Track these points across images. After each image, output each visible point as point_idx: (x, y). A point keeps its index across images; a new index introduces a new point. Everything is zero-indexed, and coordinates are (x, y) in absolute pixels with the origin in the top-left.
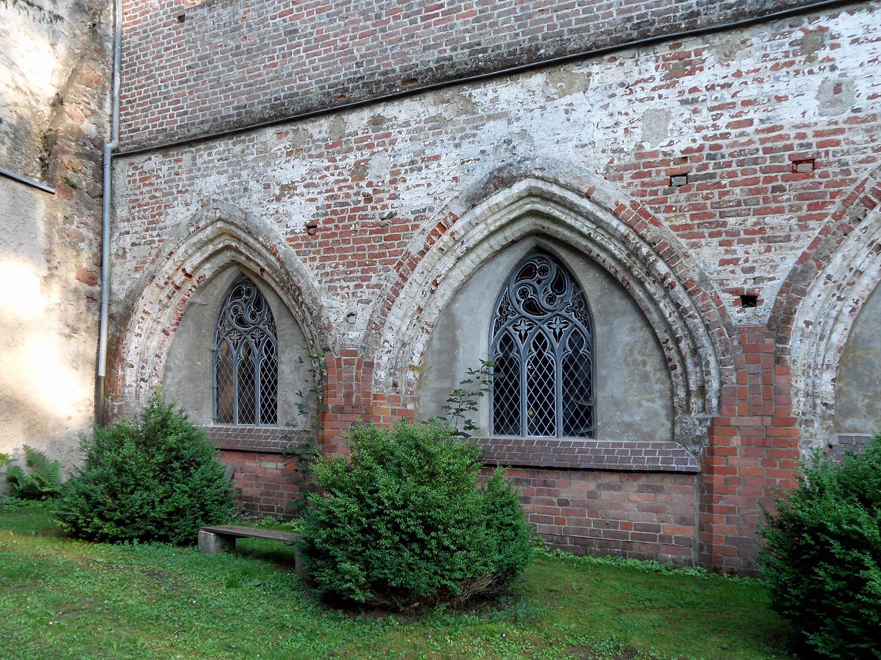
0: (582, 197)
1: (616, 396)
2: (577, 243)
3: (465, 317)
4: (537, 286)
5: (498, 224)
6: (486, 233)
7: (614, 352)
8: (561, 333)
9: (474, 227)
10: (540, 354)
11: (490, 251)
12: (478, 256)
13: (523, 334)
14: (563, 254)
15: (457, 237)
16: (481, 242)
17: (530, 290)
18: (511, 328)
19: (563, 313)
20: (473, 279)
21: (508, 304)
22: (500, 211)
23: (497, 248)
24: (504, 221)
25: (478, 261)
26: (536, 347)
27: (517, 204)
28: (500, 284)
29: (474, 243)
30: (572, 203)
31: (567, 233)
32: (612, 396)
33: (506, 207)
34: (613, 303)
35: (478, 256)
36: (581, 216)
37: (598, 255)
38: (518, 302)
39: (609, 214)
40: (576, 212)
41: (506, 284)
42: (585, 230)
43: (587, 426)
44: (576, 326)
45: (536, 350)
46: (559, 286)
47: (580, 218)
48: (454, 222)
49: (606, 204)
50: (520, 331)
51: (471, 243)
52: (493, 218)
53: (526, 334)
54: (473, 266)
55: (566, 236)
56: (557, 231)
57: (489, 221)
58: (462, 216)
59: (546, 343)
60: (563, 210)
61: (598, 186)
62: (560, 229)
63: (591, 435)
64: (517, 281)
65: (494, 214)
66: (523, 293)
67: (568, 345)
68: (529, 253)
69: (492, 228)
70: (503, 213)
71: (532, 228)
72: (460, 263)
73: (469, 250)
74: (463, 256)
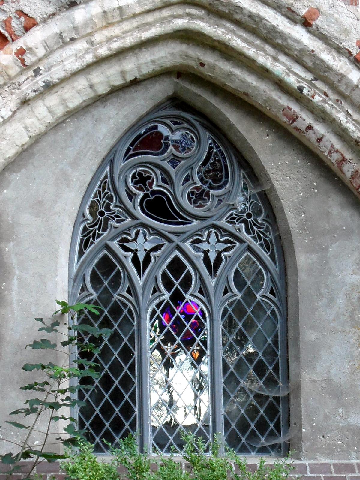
0: (294, 21)
1: (336, 380)
2: (269, 100)
3: (26, 218)
4: (172, 171)
5: (116, 45)
6: (89, 58)
7: (331, 300)
8: (219, 260)
9: (65, 44)
10: (177, 298)
11: (89, 94)
12: (64, 102)
13: (141, 257)
14: (233, 117)
15: (29, 59)
16: (75, 74)
17: (156, 176)
18: (115, 245)
19: (223, 223)
20: (44, 143)
21: (110, 199)
22: (122, 21)
23: (102, 90)
24: (129, 41)
25: (60, 111)
26: (169, 285)
27: (157, 15)
28: (98, 160)
29: (62, 74)
30: (273, 30)
31: (251, 80)
32: (329, 380)
33: (135, 16)
34: (328, 214)
35: (64, 102)
36: (286, 54)
37: (310, 127)
38: (131, 196)
39: (344, 60)
40: (275, 46)
41: (109, 160)
42: (292, 80)
43: (272, 435)
44: (250, 249)
45: (168, 289)
46: (215, 175)
47: (282, 58)
48: (27, 29)
49: (341, 41)
50: (135, 252)
51: (56, 74)
52: (108, 33)
53: (147, 259)
54: (49, 119)
55: (249, 86)
56: (230, 75)
57: (98, 37)
58: (44, 21)
59: (188, 278)
60: (251, 38)
61: (325, 8)
62: (237, 71)
63: (284, 450)
64: (127, 155)
65: (109, 25)
66: (142, 180)
67: (232, 284)
68: (158, 107)
69: (104, 51)
70: (127, 26)
71: (179, 61)
72: (25, 111)
73: (49, 87)
74: (35, 98)
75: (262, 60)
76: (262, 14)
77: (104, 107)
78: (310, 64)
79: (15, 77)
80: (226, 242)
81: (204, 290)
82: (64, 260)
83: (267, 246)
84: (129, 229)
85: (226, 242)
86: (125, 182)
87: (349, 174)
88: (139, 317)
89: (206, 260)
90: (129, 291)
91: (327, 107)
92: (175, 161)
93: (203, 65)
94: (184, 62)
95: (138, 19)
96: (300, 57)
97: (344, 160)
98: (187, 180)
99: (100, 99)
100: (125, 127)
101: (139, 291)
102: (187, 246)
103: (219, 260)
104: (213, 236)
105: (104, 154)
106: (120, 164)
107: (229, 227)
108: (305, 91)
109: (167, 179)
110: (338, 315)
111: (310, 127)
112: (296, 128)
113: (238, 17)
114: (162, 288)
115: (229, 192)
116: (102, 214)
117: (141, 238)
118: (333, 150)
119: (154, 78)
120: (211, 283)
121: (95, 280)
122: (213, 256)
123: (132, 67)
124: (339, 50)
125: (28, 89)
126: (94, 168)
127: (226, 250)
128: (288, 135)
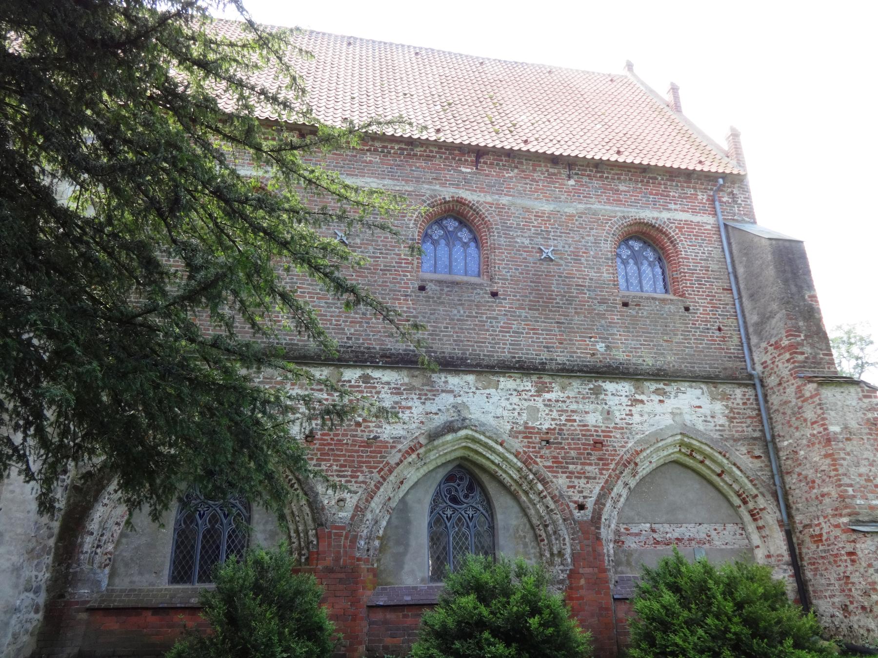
14: (477, 471)
17: (453, 490)
19: (474, 505)
42: (496, 461)
46: (471, 488)
75: (488, 455)
77: (667, 563)
81: (468, 527)
83: (487, 512)
86: (444, 492)
92: (459, 485)
94: (308, 369)
96: (498, 454)
99: (439, 467)
102: (463, 512)
106: (442, 486)
109: (456, 490)
120: (471, 524)
123: (449, 458)
124: (511, 452)
128: (494, 477)
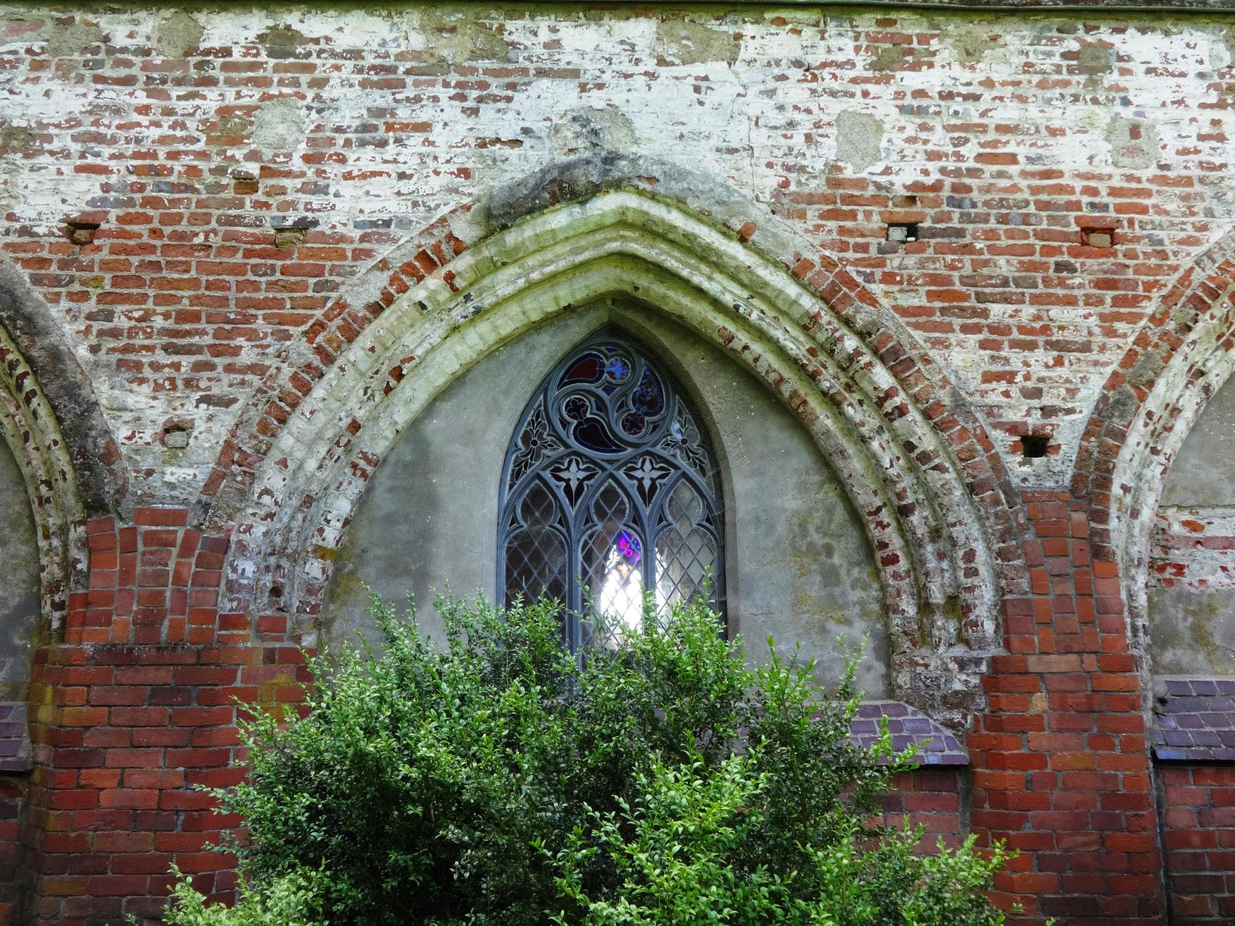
6: (521, 283)
14: (667, 341)
17: (590, 403)
18: (547, 475)
19: (658, 449)
23: (535, 316)
24: (562, 265)
25: (492, 338)
27: (591, 238)
28: (530, 390)
37: (746, 347)
38: (565, 424)
41: (543, 388)
42: (728, 299)
44: (684, 475)
47: (717, 276)
48: (457, 252)
51: (488, 300)
54: (481, 346)
56: (664, 297)
64: (562, 384)
66: (576, 408)
68: (593, 334)
69: (535, 276)
70: (559, 249)
71: (613, 286)
72: (456, 337)
75: (697, 279)
76: (697, 231)
78: (746, 281)
79: (445, 303)
80: (661, 469)
82: (493, 491)
84: (562, 458)
85: (661, 469)
87: (787, 395)
88: (570, 550)
89: (641, 488)
90: (560, 522)
91: (764, 325)
93: (636, 289)
95: (572, 241)
97: (782, 380)
98: (621, 407)
100: (560, 355)
101: (571, 522)
102: (621, 474)
103: (653, 488)
104: (647, 463)
105: (537, 382)
106: (554, 393)
107: (665, 454)
108: (741, 310)
109: (601, 406)
110: (778, 543)
111: (746, 347)
112: (732, 350)
113: (671, 236)
114: (595, 517)
115: (664, 418)
116: (535, 443)
117: (573, 467)
118: (770, 370)
119: (563, 279)
121: (526, 510)
122: (647, 484)
123: (567, 294)
124: (776, 264)
125: (457, 314)
126: (528, 396)
127: (662, 477)
128: (725, 357)
